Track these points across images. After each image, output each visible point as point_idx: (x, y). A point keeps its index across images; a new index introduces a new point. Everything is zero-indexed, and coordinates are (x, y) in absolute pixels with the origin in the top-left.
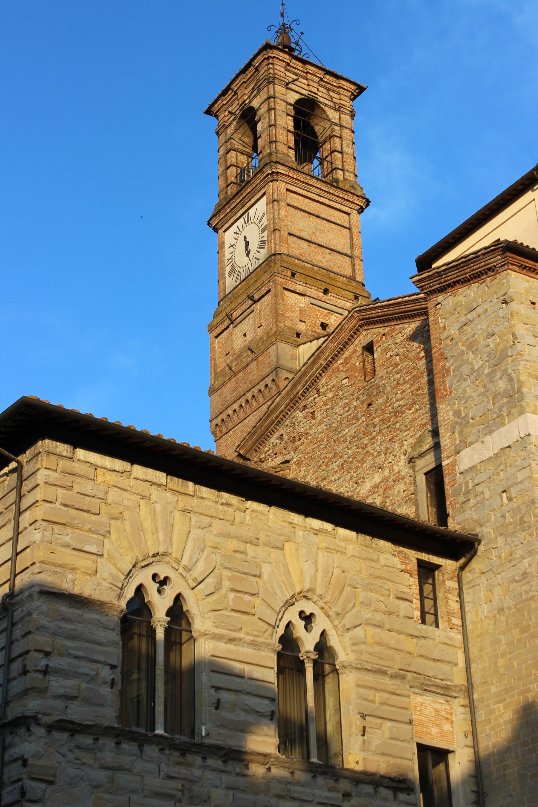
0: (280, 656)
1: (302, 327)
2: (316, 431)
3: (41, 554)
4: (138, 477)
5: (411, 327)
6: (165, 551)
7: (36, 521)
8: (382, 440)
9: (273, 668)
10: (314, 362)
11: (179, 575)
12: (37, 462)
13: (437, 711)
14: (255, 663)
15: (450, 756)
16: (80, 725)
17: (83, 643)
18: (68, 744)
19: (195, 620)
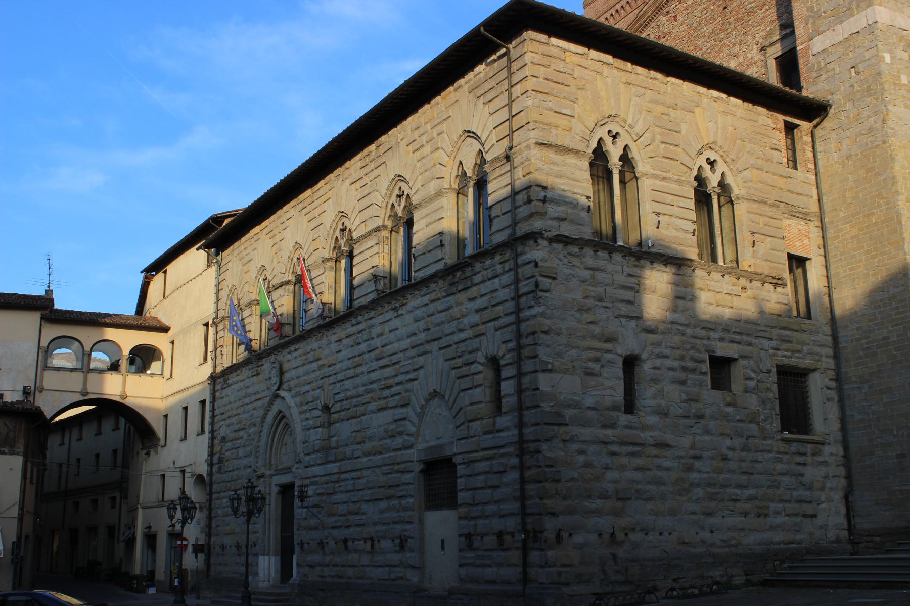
0: (696, 191)
13: (799, 230)
15: (808, 262)
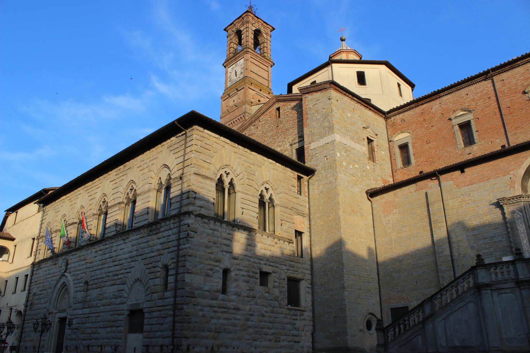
0: (259, 200)
1: (253, 100)
5: (293, 104)
10: (259, 112)
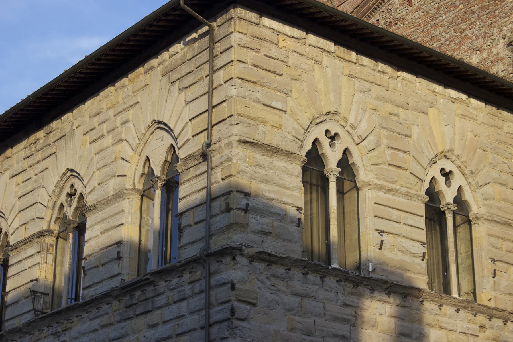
0: (427, 206)
2: (413, 17)
3: (238, 108)
4: (312, 43)
6: (336, 110)
7: (232, 78)
8: (480, 26)
9: (422, 216)
11: (346, 132)
12: (230, 26)
14: (409, 211)
16: (276, 256)
17: (274, 187)
18: (266, 273)
19: (360, 172)
